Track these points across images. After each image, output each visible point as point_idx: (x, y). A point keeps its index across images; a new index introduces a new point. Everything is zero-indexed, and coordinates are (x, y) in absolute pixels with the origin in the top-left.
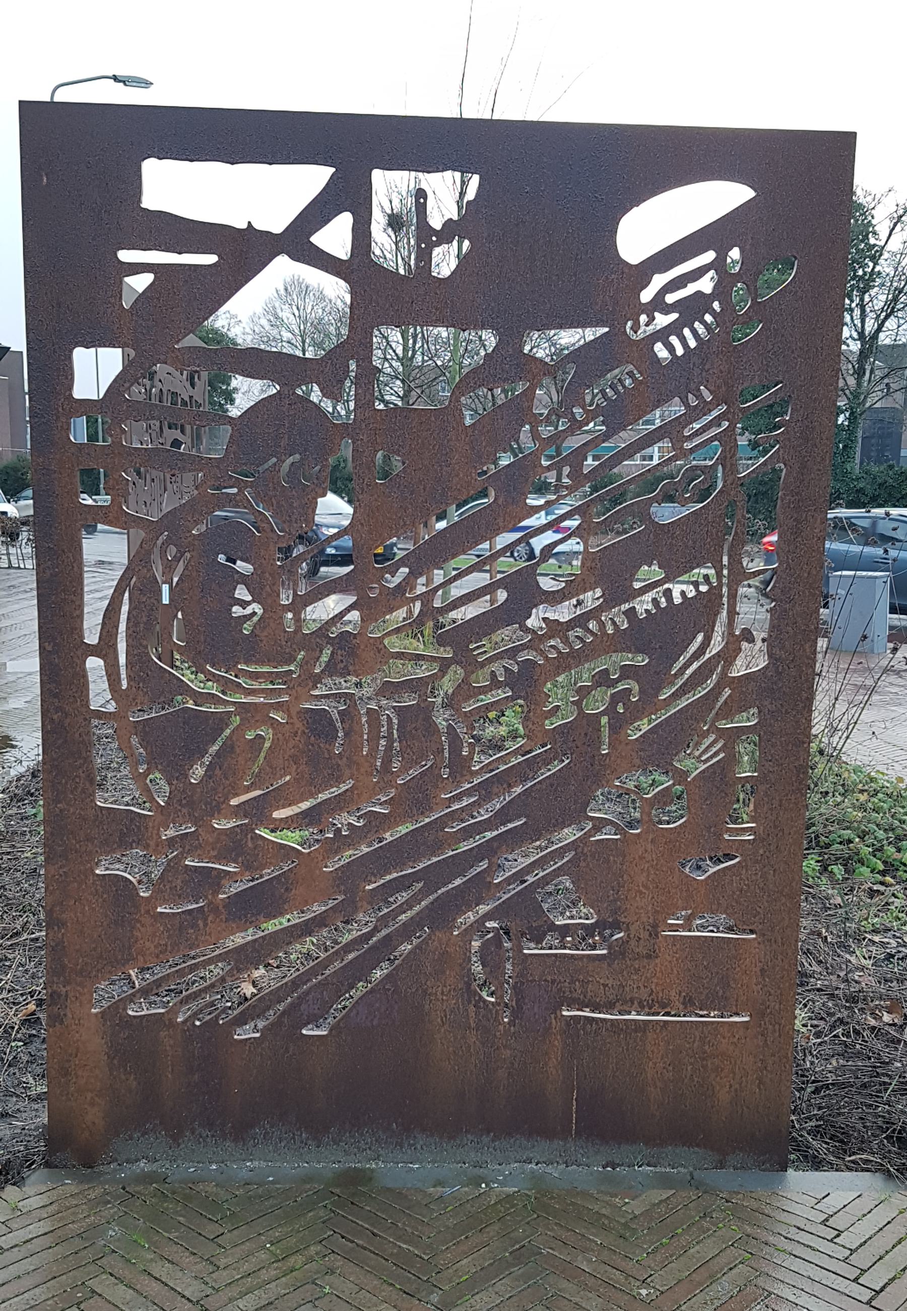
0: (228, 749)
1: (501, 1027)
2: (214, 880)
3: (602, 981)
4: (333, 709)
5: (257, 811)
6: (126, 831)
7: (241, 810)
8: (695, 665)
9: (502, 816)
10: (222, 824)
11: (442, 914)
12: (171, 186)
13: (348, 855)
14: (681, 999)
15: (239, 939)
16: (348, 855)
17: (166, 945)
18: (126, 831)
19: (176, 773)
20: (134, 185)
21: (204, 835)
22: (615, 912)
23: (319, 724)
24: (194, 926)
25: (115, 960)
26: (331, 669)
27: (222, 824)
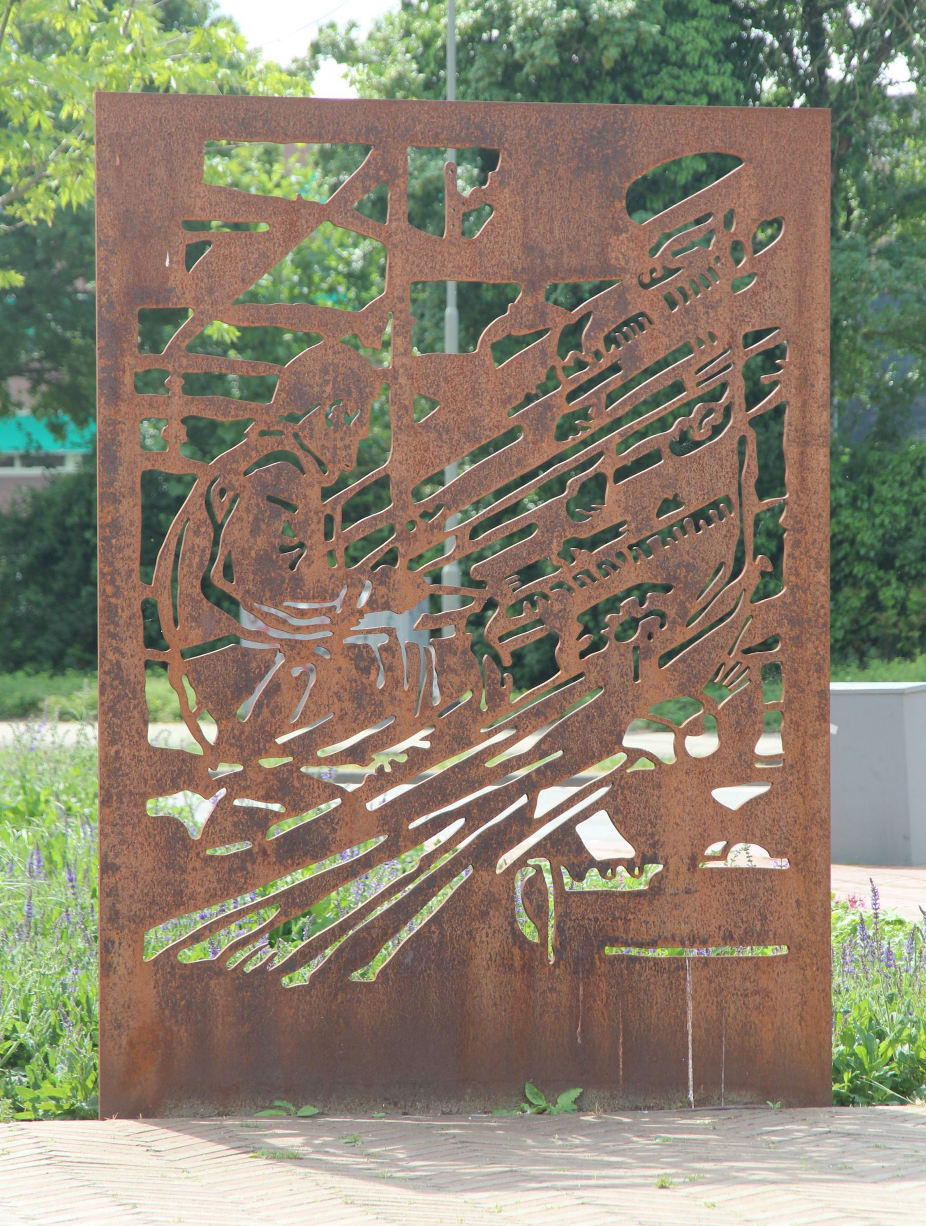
0: (273, 689)
1: (546, 970)
2: (263, 820)
3: (643, 919)
4: (377, 642)
5: (303, 750)
6: (180, 771)
7: (286, 749)
8: (386, 906)
9: (538, 751)
10: (269, 763)
11: (486, 851)
12: (233, 166)
13: (392, 794)
14: (722, 933)
15: (285, 883)
16: (392, 794)
17: (215, 889)
18: (180, 771)
19: (223, 715)
20: (785, 745)
21: (251, 774)
22: (653, 846)
23: (362, 659)
24: (243, 868)
25: (177, 902)
26: (372, 605)
27: (269, 763)
